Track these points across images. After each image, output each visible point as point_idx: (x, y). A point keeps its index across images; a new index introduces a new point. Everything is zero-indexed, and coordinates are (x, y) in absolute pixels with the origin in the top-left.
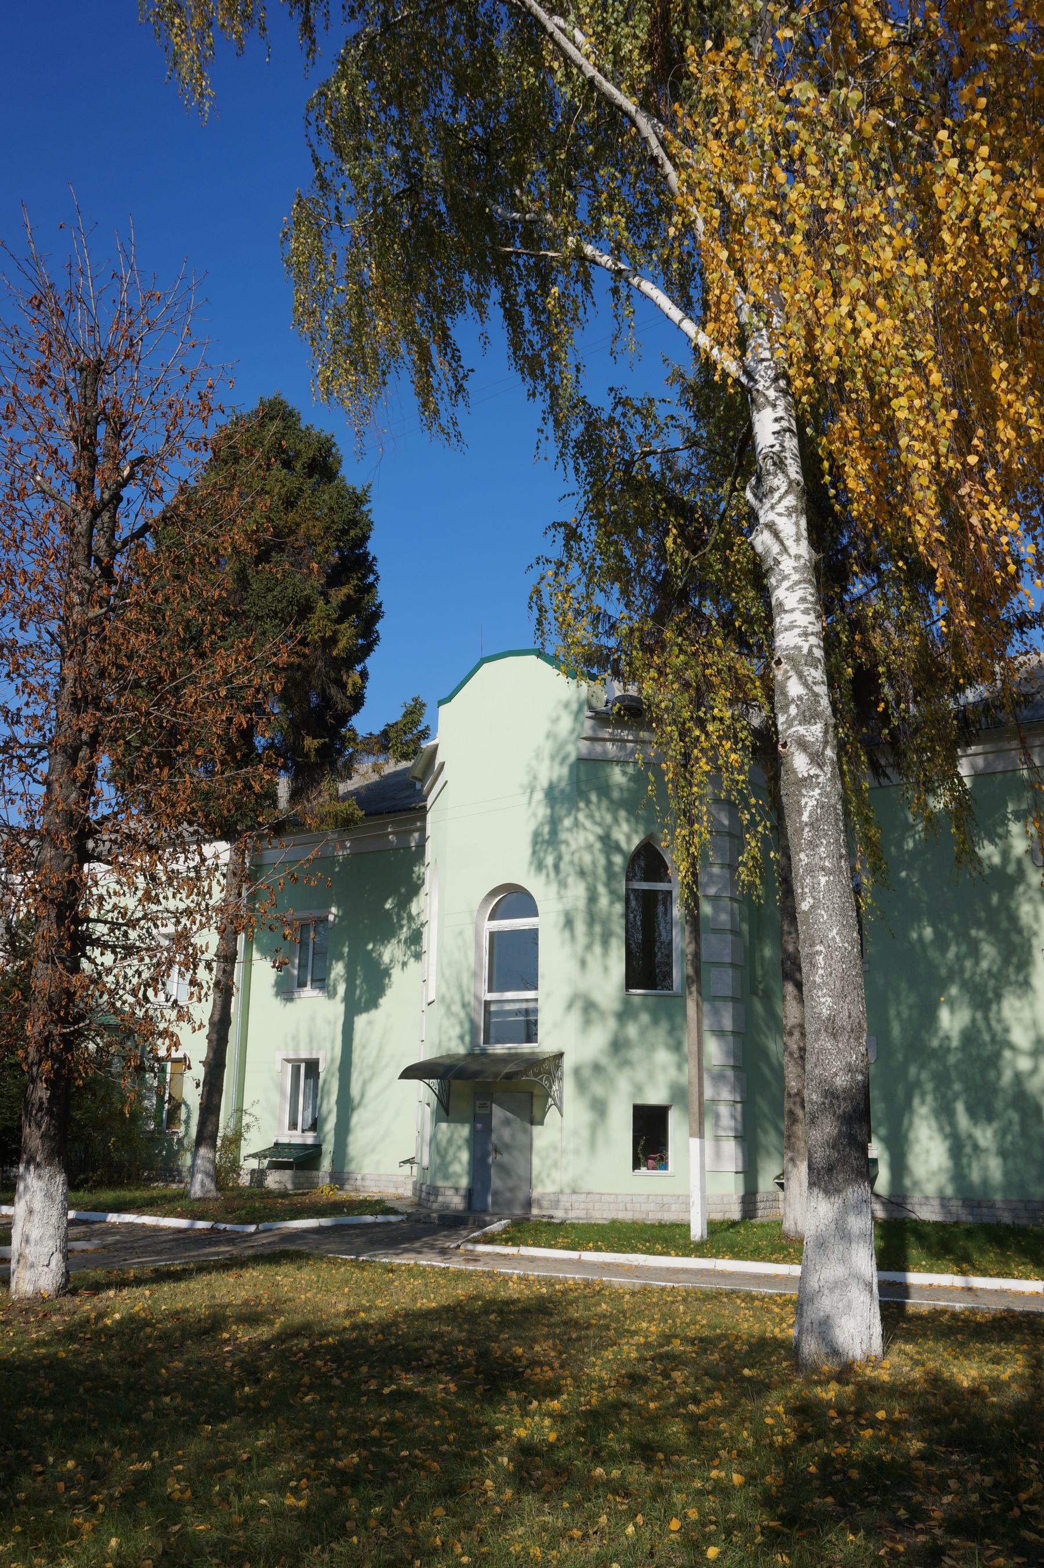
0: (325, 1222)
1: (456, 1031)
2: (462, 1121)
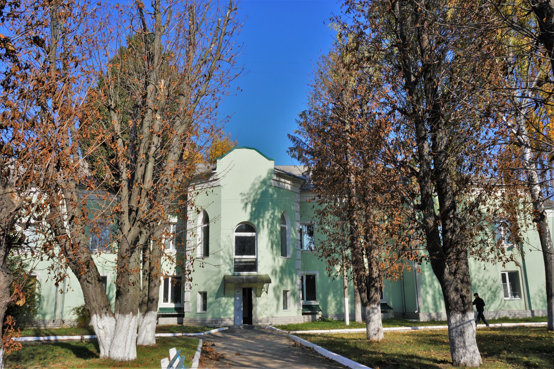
2: (231, 297)
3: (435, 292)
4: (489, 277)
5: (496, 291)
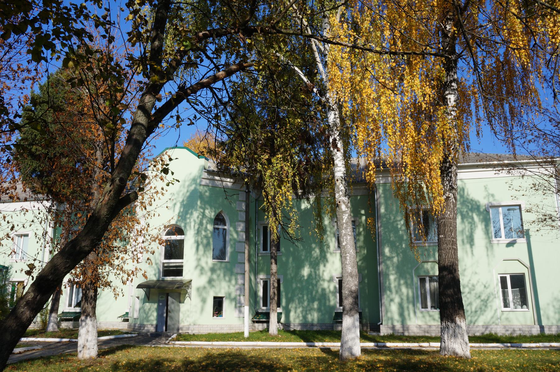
0: (112, 337)
1: (153, 272)
2: (154, 302)
3: (402, 299)
4: (478, 282)
5: (487, 300)
